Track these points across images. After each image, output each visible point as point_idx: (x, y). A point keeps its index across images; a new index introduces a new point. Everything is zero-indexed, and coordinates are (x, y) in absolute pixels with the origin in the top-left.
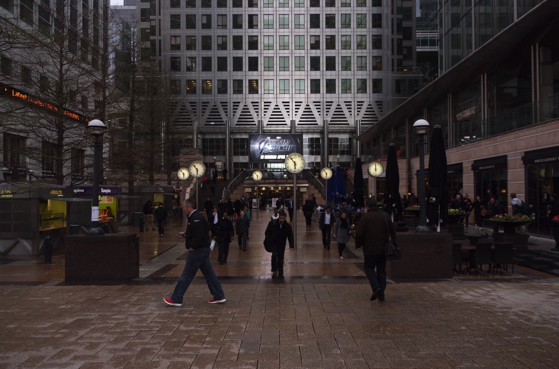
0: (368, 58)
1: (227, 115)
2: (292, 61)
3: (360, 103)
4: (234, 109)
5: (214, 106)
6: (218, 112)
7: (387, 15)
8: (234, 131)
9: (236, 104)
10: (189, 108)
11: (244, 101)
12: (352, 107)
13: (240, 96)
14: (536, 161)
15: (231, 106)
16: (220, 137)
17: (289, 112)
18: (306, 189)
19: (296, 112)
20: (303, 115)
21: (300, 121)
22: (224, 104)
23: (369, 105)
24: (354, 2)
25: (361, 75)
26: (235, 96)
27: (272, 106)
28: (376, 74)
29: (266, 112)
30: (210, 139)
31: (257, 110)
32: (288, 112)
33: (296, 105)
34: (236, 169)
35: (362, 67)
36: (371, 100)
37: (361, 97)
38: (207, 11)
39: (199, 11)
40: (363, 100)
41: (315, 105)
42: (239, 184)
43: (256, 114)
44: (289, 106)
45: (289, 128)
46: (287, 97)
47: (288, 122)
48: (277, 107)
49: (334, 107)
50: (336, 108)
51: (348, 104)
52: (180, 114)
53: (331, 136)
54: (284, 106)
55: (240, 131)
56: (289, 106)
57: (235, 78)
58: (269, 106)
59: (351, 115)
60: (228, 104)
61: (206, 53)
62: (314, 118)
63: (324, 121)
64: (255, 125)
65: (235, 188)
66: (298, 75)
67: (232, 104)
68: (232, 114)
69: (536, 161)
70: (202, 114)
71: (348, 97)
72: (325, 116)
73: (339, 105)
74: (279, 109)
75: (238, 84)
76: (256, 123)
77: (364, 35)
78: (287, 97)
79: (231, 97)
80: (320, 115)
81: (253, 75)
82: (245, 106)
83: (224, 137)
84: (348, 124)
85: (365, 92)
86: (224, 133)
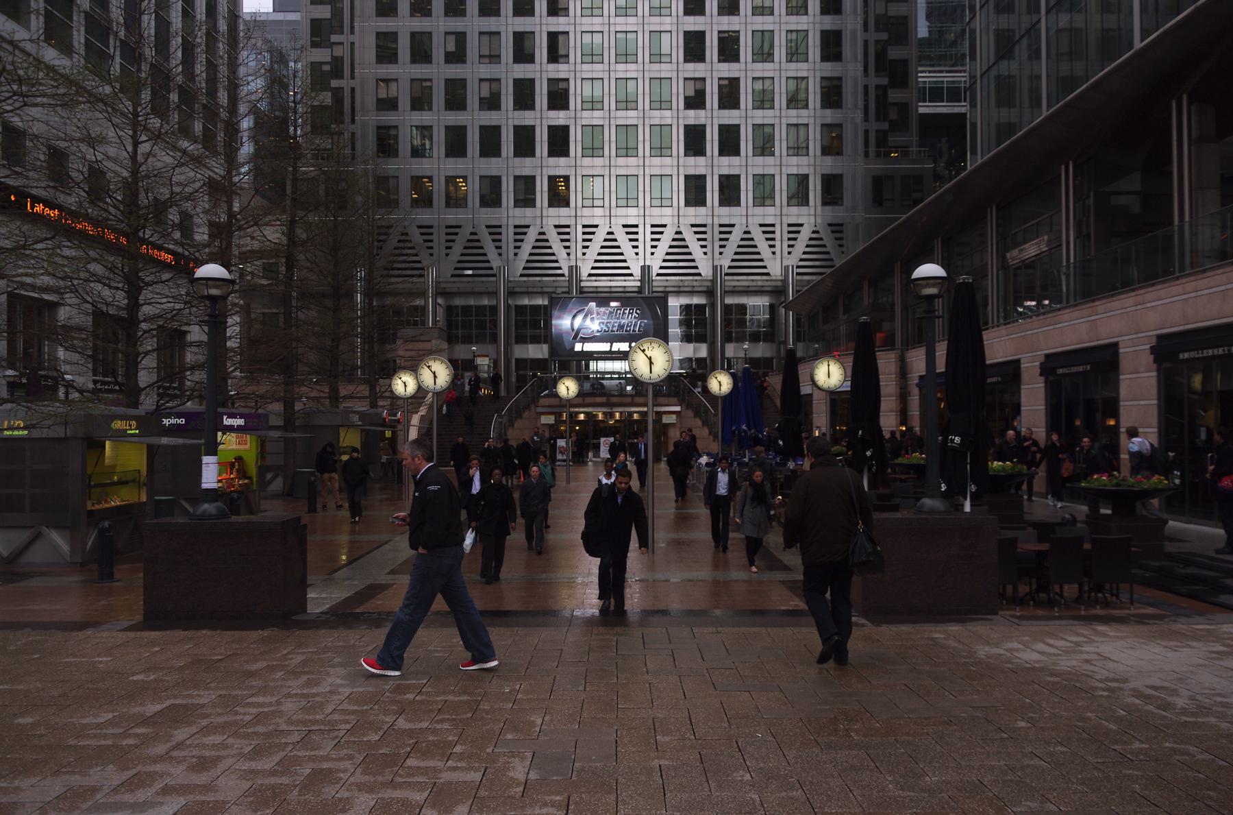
0: (811, 128)
1: (500, 255)
2: (644, 135)
3: (795, 228)
4: (516, 241)
5: (472, 234)
6: (482, 248)
7: (854, 33)
8: (517, 290)
9: (521, 230)
10: (418, 238)
11: (538, 222)
12: (777, 235)
13: (528, 211)
14: (1181, 356)
15: (509, 235)
16: (486, 302)
17: (636, 247)
18: (674, 416)
19: (653, 247)
20: (668, 254)
21: (661, 268)
22: (495, 231)
23: (814, 232)
24: (780, 5)
25: (797, 165)
26: (519, 212)
27: (601, 235)
28: (829, 164)
29: (587, 247)
30: (463, 307)
31: (567, 244)
32: (634, 247)
33: (652, 233)
34: (521, 372)
35: (798, 149)
36: (819, 220)
37: (796, 214)
38: (456, 24)
39: (439, 24)
40: (800, 222)
41: (696, 233)
42: (527, 407)
43: (564, 252)
44: (637, 233)
45: (639, 284)
46: (632, 215)
47: (636, 270)
48: (610, 237)
49: (736, 236)
50: (742, 239)
51: (768, 229)
52: (397, 252)
53: (729, 300)
54: (627, 233)
55: (530, 290)
56: (637, 233)
57: (518, 173)
58: (593, 233)
59: (774, 253)
60: (503, 230)
61: (455, 118)
62: (693, 261)
63: (715, 268)
64: (563, 275)
65: (519, 416)
66: (658, 165)
67: (511, 230)
68: (512, 251)
69: (1181, 356)
70: (445, 251)
71: (769, 214)
72: (717, 255)
73: (749, 232)
74: (615, 240)
75: (526, 186)
76: (565, 271)
77: (803, 78)
78: (632, 215)
79: (510, 214)
80: (705, 253)
81: (559, 166)
82: (540, 234)
83: (494, 303)
84: (768, 274)
85: (806, 203)
86: (495, 294)
